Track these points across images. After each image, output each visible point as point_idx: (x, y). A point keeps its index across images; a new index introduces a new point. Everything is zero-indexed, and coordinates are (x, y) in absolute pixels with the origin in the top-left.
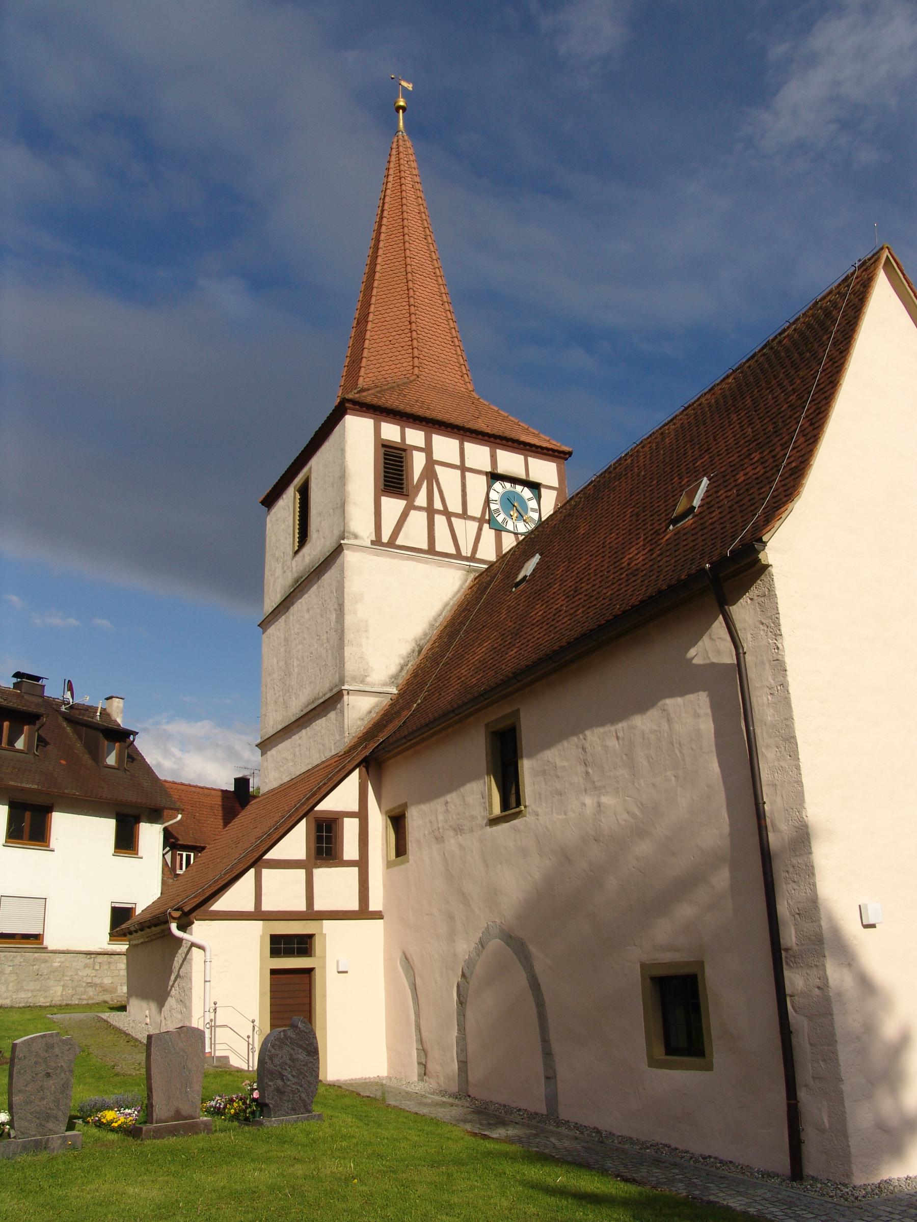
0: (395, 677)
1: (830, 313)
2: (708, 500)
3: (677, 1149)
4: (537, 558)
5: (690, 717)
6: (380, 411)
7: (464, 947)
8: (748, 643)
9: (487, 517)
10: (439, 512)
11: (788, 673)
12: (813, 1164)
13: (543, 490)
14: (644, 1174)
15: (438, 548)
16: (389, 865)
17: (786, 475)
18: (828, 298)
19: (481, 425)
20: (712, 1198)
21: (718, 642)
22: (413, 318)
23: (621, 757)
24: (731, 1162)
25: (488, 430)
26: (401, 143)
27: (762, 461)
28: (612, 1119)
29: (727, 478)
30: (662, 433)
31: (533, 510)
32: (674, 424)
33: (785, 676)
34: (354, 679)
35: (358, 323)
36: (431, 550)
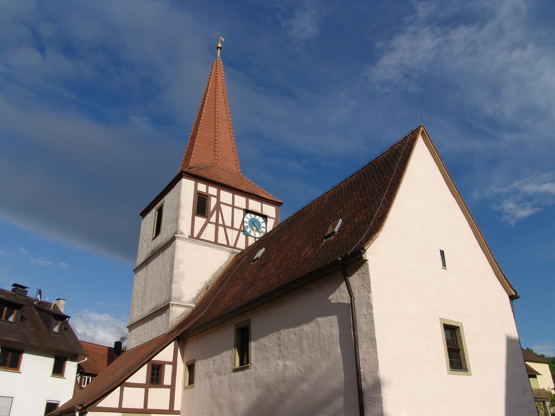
0: (195, 299)
4: (264, 249)
5: (328, 326)
8: (356, 294)
10: (221, 225)
13: (268, 219)
15: (219, 242)
16: (185, 388)
19: (243, 188)
25: (246, 190)
31: (263, 227)
33: (372, 310)
34: (176, 299)
36: (216, 242)
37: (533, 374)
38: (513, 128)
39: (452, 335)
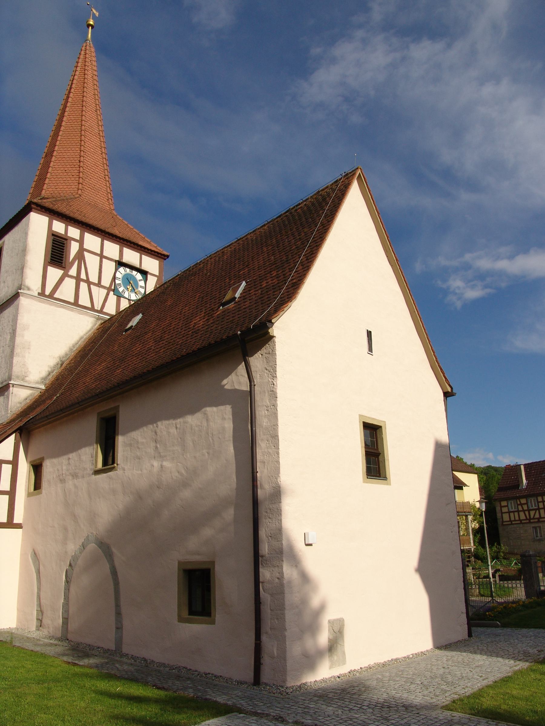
0: (44, 379)
1: (325, 199)
2: (244, 294)
3: (190, 669)
4: (140, 316)
5: (219, 419)
6: (53, 213)
7: (72, 547)
8: (257, 380)
9: (113, 288)
10: (83, 280)
11: (278, 399)
12: (266, 676)
13: (149, 276)
14: (170, 684)
15: (80, 303)
16: (29, 495)
17: (290, 286)
18: (325, 190)
19: (116, 231)
20: (208, 697)
21: (240, 377)
22: (82, 159)
23: (177, 439)
24: (221, 676)
25: (120, 235)
26: (88, 47)
27: (277, 277)
28: (155, 654)
29: (257, 283)
30: (223, 252)
31: (141, 287)
32: (231, 248)
33: (276, 401)
34: (18, 377)
35: (46, 156)
36: (76, 303)
37: (459, 485)
38: (473, 186)
39: (372, 436)
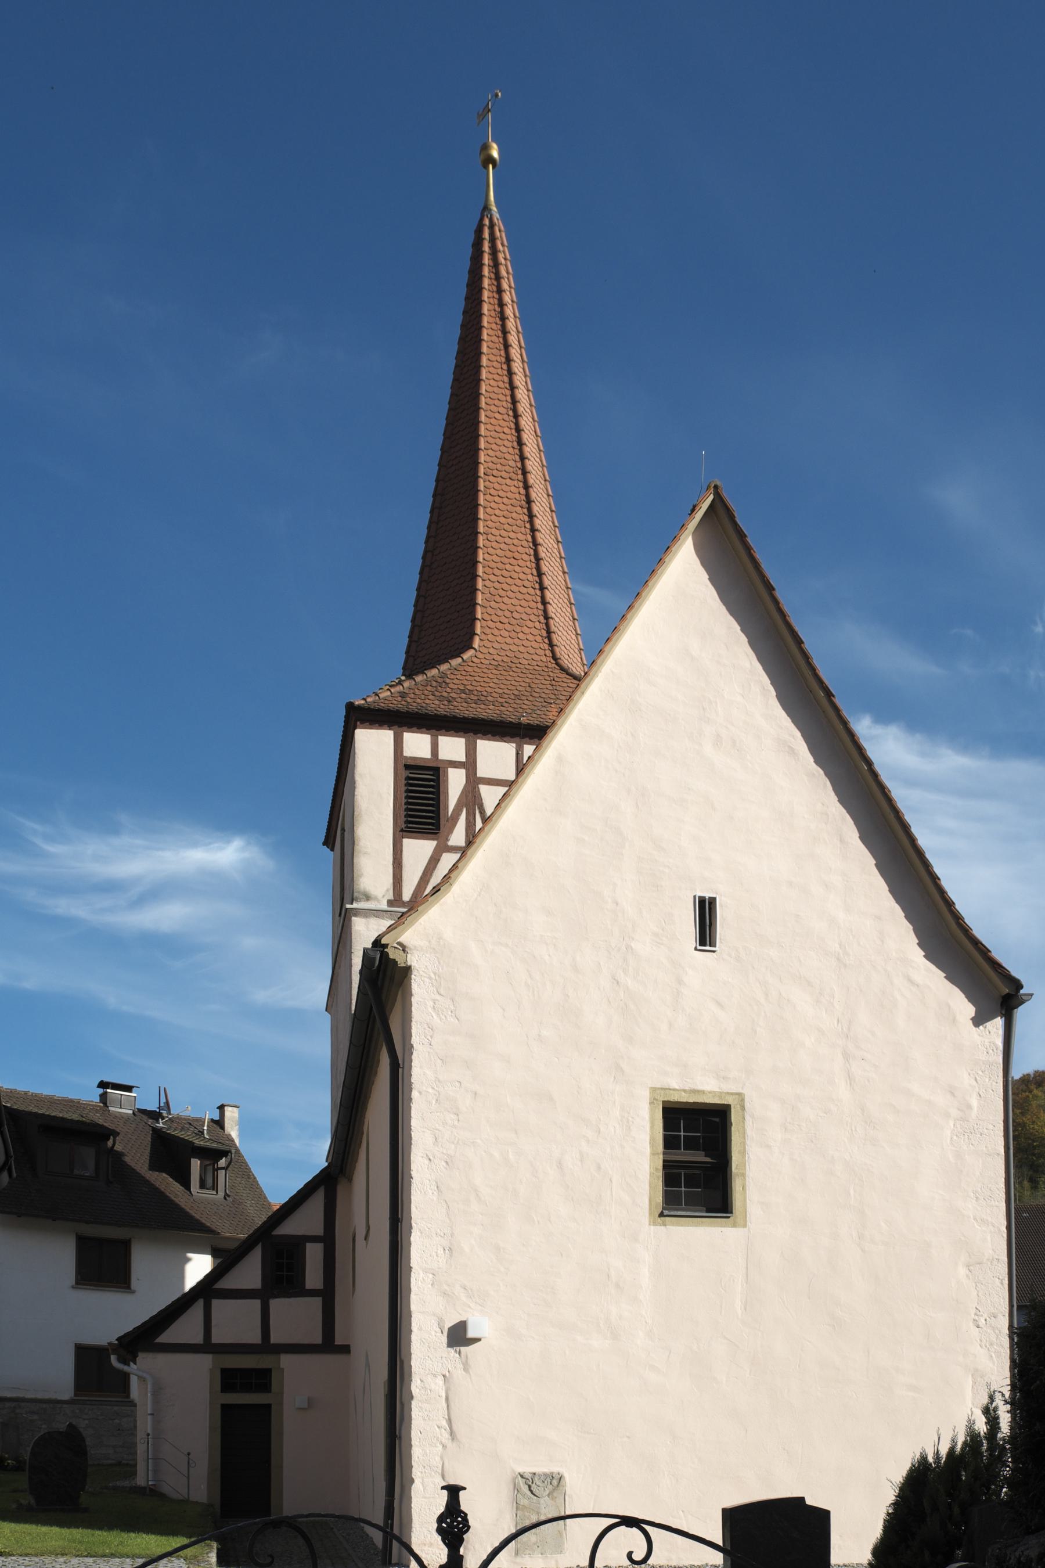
6: (398, 719)
